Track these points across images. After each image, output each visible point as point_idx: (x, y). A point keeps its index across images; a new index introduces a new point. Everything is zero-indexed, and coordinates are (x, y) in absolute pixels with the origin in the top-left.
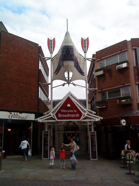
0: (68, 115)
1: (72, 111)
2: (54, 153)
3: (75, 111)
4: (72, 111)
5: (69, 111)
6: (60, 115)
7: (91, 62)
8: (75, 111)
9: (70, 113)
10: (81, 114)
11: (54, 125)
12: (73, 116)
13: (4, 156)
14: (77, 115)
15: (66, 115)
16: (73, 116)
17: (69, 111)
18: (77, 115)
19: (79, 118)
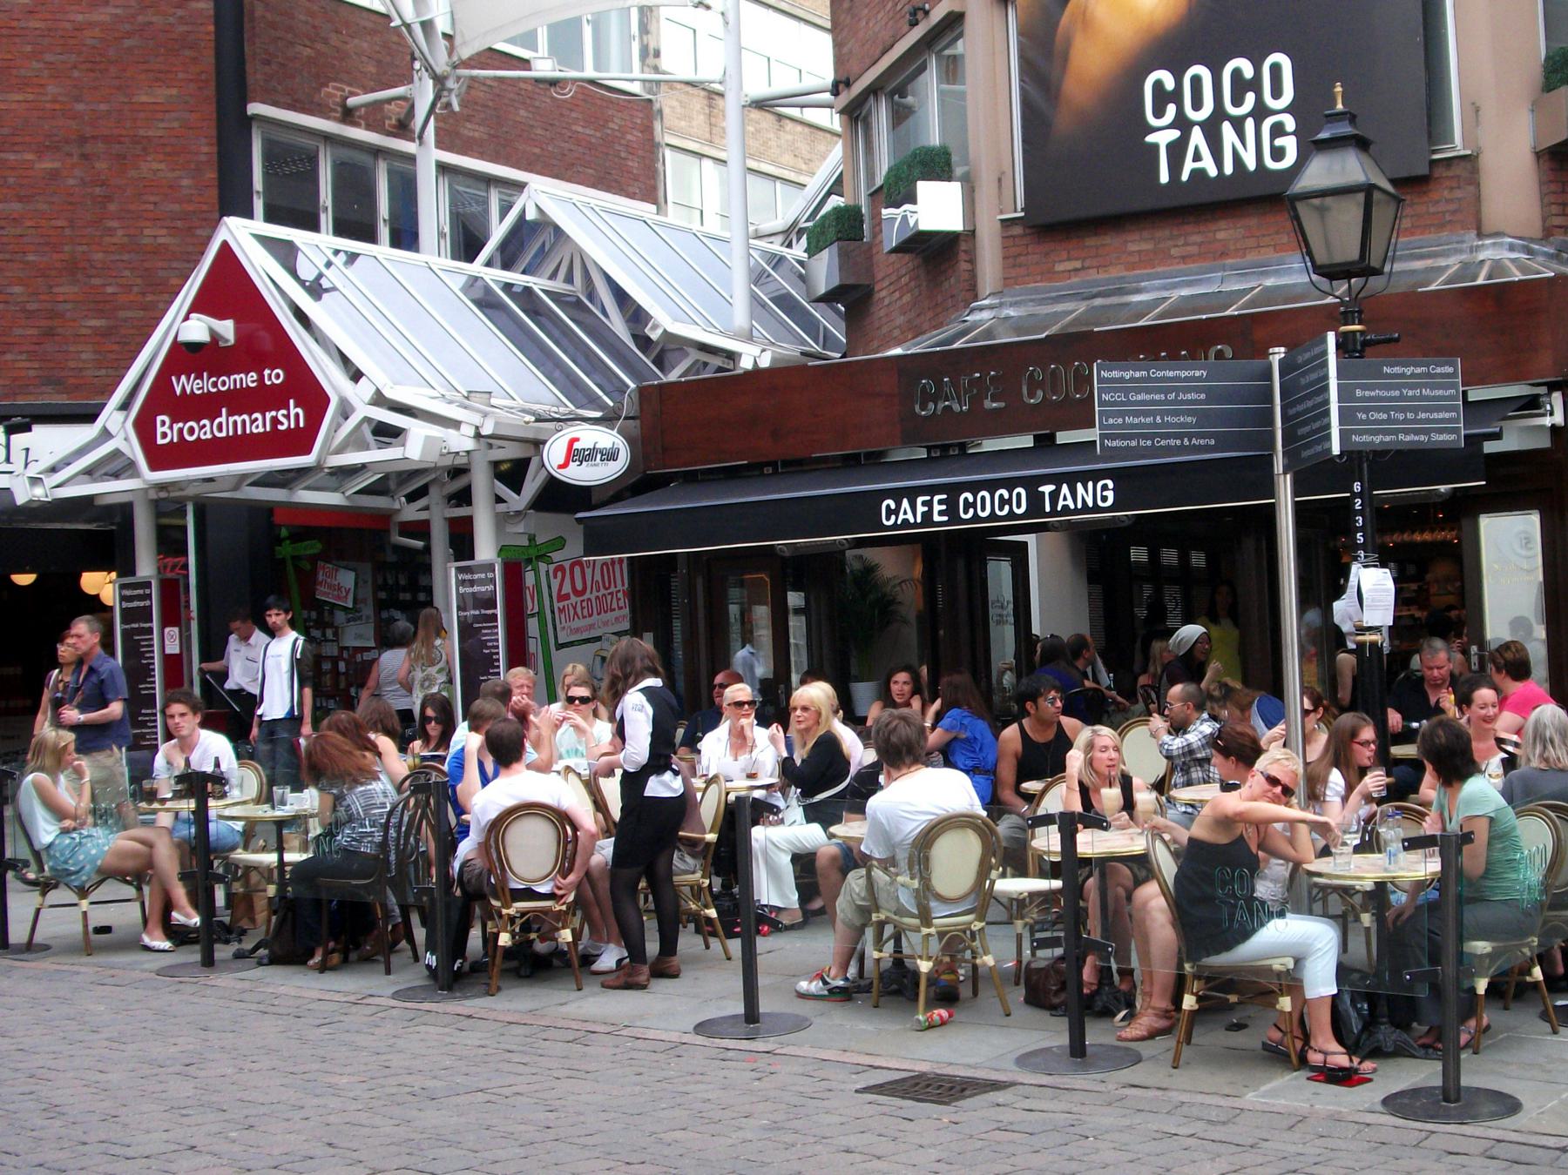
0: (226, 424)
1: (250, 380)
2: (123, 775)
3: (275, 376)
4: (250, 380)
5: (229, 382)
6: (166, 430)
7: (762, 944)
8: (275, 376)
9: (241, 401)
10: (314, 399)
11: (462, 512)
12: (258, 424)
13: (125, 700)
14: (292, 416)
15: (173, 421)
16: (258, 424)
17: (229, 382)
18: (292, 416)
19: (300, 441)
